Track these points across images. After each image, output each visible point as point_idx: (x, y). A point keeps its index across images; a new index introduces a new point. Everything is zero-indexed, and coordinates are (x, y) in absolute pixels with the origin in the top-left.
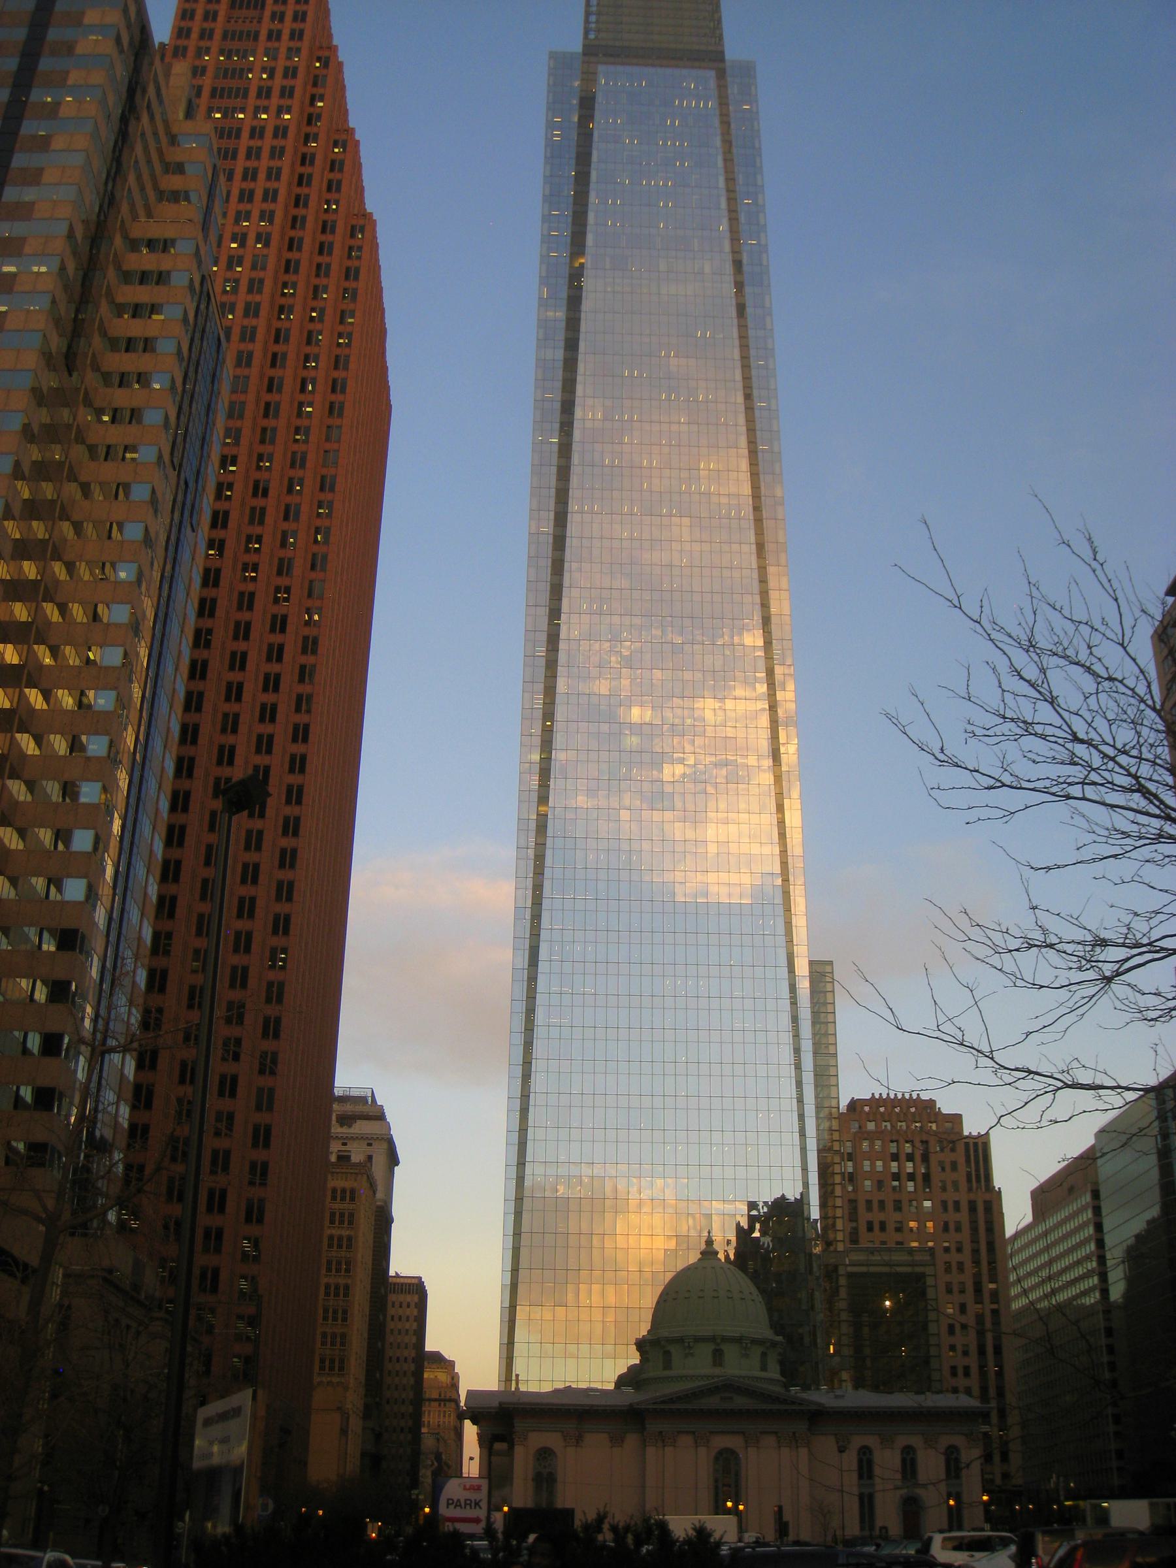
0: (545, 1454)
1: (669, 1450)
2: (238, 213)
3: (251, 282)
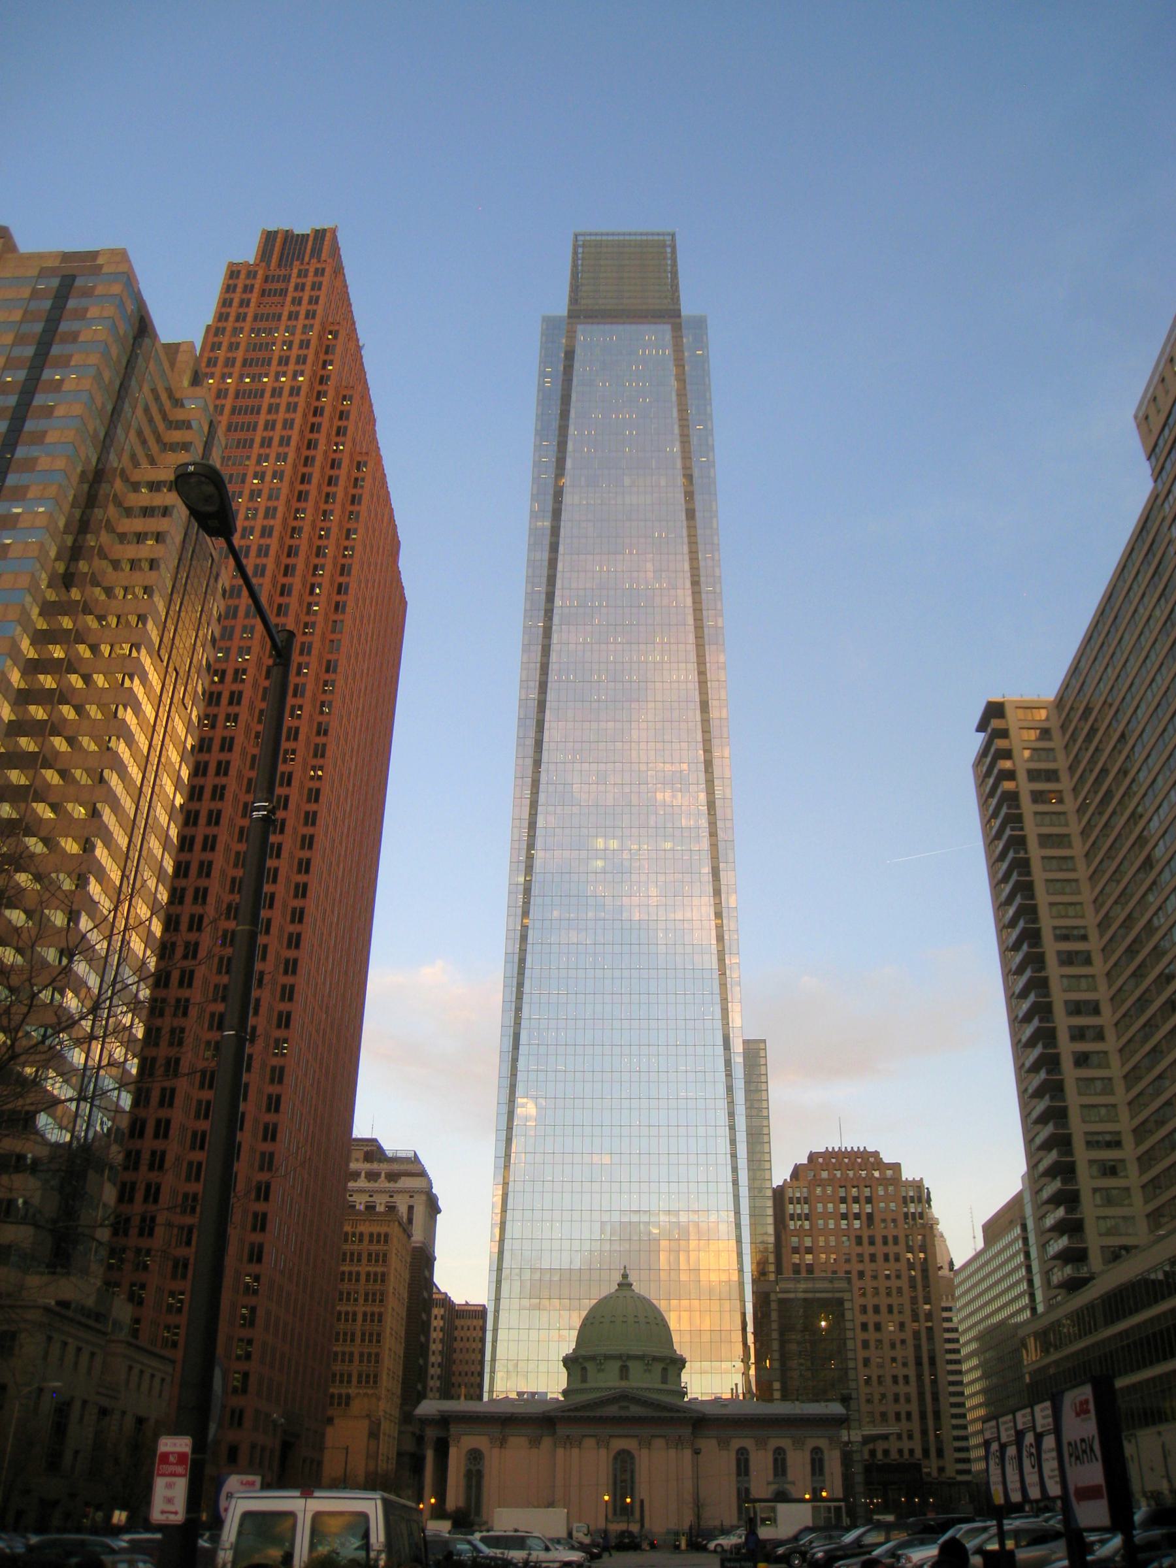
0: (475, 1456)
1: (575, 1451)
2: (260, 456)
3: (267, 509)
